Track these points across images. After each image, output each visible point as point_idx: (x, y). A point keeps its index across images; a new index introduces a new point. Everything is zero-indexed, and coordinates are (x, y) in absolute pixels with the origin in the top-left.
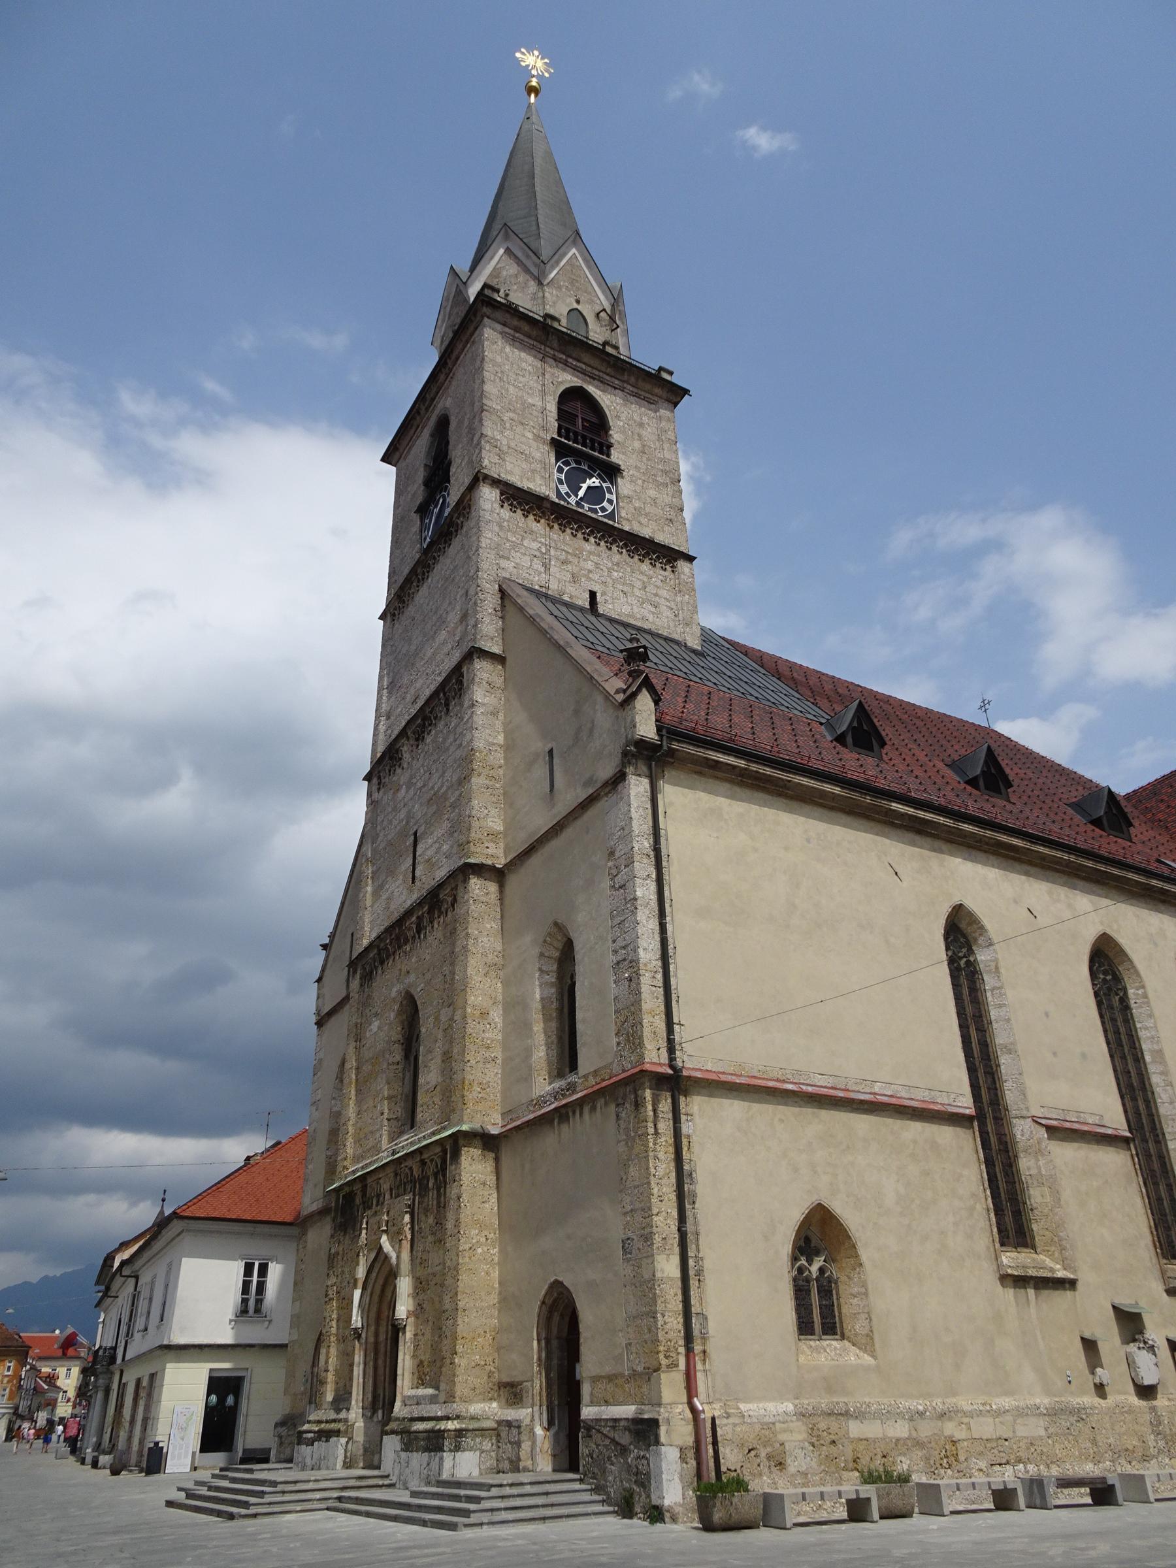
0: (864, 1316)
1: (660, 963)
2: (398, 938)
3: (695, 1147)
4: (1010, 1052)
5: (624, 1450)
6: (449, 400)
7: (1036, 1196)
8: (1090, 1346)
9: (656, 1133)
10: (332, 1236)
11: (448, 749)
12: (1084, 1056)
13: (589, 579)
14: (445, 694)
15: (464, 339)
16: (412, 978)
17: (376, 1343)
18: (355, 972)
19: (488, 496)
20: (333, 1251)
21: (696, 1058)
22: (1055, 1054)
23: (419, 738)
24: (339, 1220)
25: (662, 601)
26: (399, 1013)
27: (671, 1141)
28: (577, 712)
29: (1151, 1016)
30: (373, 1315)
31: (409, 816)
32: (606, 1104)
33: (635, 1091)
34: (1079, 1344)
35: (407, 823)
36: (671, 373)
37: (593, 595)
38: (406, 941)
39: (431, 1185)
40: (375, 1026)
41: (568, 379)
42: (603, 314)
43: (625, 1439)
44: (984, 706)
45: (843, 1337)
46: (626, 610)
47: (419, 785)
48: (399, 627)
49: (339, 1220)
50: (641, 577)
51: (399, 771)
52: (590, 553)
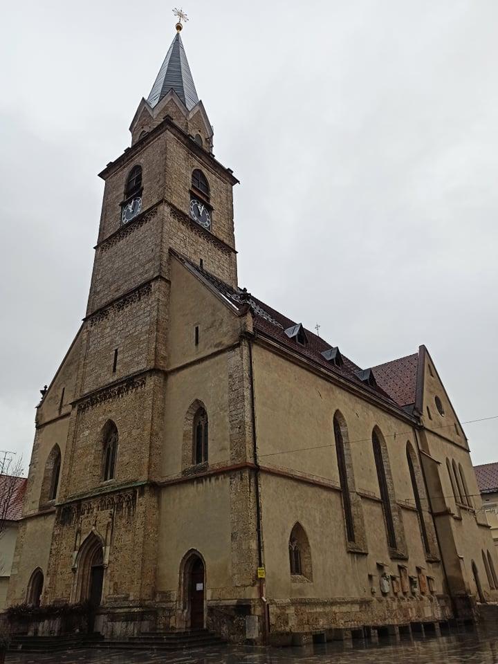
0: (309, 566)
2: (105, 395)
4: (350, 467)
5: (232, 618)
6: (142, 161)
8: (370, 577)
9: (250, 491)
10: (55, 526)
14: (139, 292)
16: (113, 414)
17: (83, 575)
18: (75, 407)
19: (166, 210)
20: (55, 533)
21: (262, 463)
22: (363, 469)
23: (120, 307)
24: (60, 519)
28: (213, 315)
29: (388, 457)
32: (224, 478)
34: (367, 576)
37: (201, 260)
39: (124, 506)
40: (87, 433)
41: (197, 165)
43: (233, 613)
44: (317, 327)
48: (106, 255)
51: (105, 320)
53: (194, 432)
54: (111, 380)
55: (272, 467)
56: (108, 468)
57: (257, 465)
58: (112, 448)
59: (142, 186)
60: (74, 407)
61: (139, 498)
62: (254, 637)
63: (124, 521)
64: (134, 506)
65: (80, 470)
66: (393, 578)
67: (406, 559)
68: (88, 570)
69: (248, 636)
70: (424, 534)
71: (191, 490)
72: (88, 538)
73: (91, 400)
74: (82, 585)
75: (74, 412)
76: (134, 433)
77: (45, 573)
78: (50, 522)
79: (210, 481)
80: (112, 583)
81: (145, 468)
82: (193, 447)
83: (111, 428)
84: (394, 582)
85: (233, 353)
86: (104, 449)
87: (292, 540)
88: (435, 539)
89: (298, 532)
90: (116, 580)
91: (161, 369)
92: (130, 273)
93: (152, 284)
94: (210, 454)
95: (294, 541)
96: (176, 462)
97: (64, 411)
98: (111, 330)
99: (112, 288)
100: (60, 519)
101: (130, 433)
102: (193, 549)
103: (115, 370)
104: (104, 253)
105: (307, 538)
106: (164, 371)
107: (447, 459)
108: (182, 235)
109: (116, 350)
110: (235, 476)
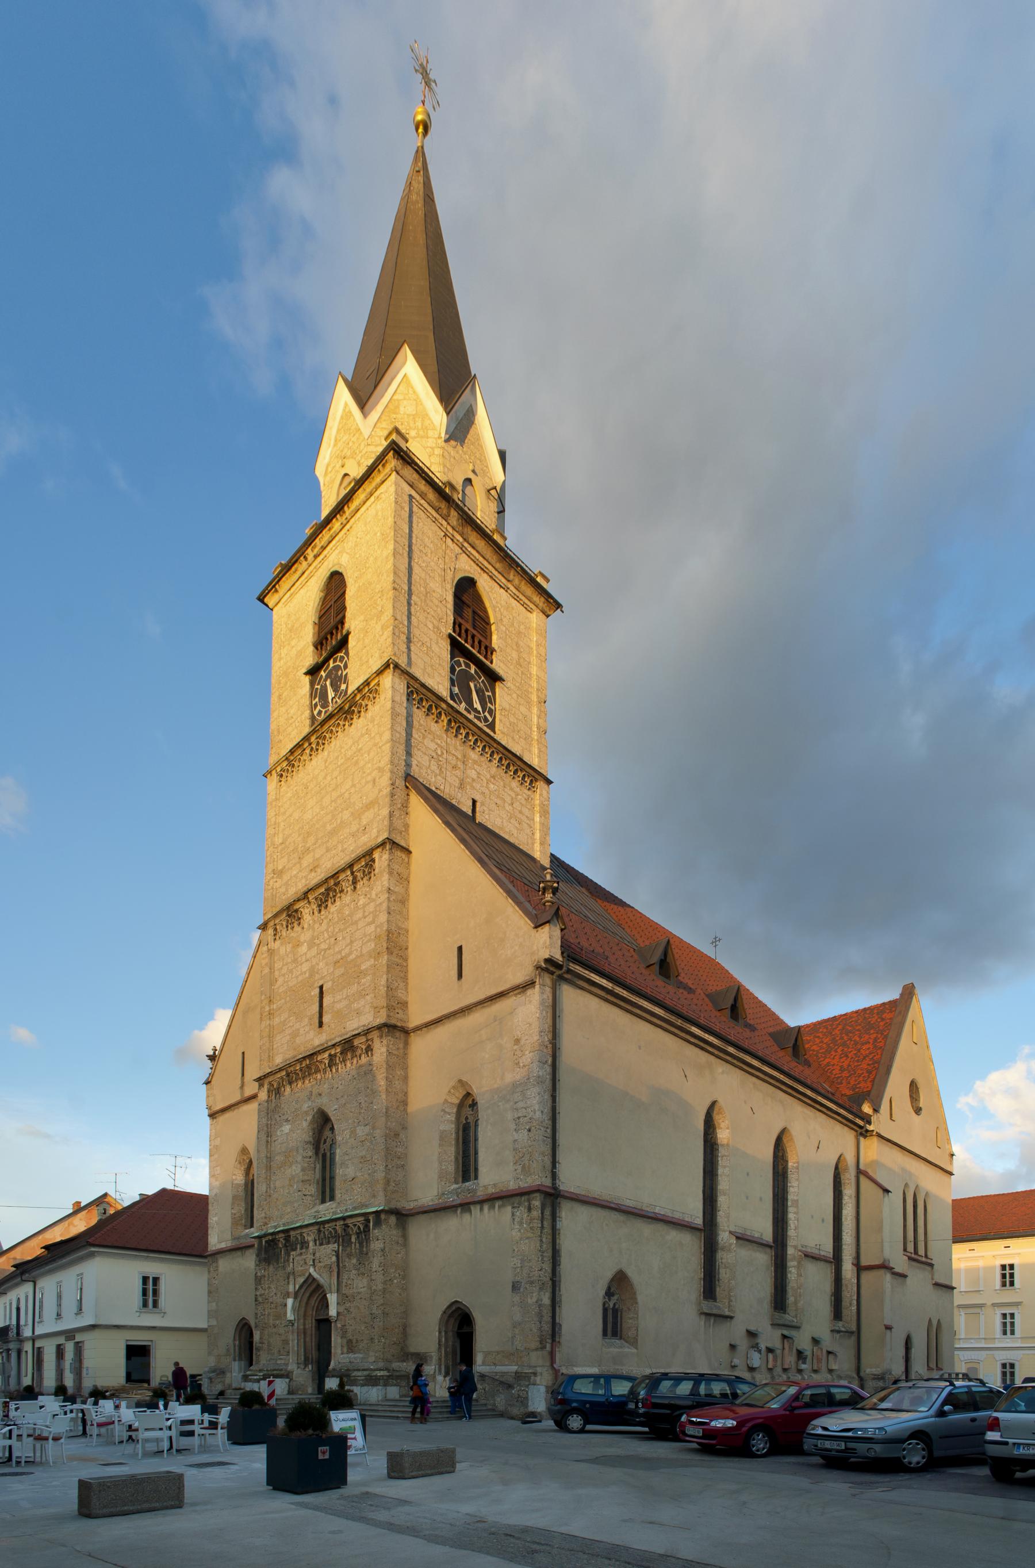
1: (550, 1122)
2: (308, 1067)
3: (562, 1237)
7: (723, 1274)
8: (733, 1347)
11: (356, 923)
12: (761, 1199)
13: (473, 788)
14: (352, 873)
15: (368, 490)
17: (305, 1329)
21: (570, 1180)
23: (322, 903)
25: (525, 819)
26: (311, 1123)
27: (550, 1232)
30: (302, 1312)
31: (312, 971)
33: (529, 1201)
35: (311, 976)
36: (547, 580)
37: (474, 802)
38: (318, 1071)
39: (353, 1240)
41: (467, 567)
42: (493, 492)
45: (621, 1338)
46: (498, 822)
47: (323, 946)
49: (263, 1256)
50: (511, 793)
51: (297, 928)
52: (475, 762)
53: (457, 1133)
54: (317, 1042)
55: (583, 1193)
56: (326, 1191)
57: (554, 1187)
58: (328, 1154)
59: (346, 626)
60: (261, 1086)
61: (374, 1229)
62: (539, 1410)
63: (354, 1261)
64: (368, 1240)
65: (283, 1187)
66: (770, 1350)
67: (797, 1328)
68: (311, 1324)
69: (531, 1409)
70: (905, 1226)
71: (452, 1223)
72: (305, 1282)
73: (288, 1075)
74: (305, 1342)
75: (263, 1095)
76: (361, 1131)
77: (253, 1325)
78: (249, 1261)
79: (481, 1209)
80: (345, 1341)
81: (380, 1187)
82: (456, 1159)
83: (323, 1122)
84: (770, 1356)
85: (521, 998)
86: (317, 1154)
87: (609, 1294)
88: (855, 1302)
89: (619, 1284)
90: (349, 1336)
91: (399, 1024)
92: (334, 832)
93: (376, 855)
94: (483, 1170)
95: (613, 1295)
96: (428, 1178)
97: (248, 1092)
98: (309, 949)
99: (305, 863)
100: (263, 1256)
101: (353, 1132)
102: (456, 1302)
103: (321, 1024)
104: (284, 788)
105: (635, 1293)
106: (402, 1027)
107: (906, 1185)
108: (433, 746)
109: (321, 987)
110: (520, 1204)
